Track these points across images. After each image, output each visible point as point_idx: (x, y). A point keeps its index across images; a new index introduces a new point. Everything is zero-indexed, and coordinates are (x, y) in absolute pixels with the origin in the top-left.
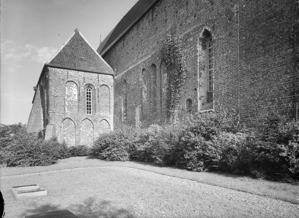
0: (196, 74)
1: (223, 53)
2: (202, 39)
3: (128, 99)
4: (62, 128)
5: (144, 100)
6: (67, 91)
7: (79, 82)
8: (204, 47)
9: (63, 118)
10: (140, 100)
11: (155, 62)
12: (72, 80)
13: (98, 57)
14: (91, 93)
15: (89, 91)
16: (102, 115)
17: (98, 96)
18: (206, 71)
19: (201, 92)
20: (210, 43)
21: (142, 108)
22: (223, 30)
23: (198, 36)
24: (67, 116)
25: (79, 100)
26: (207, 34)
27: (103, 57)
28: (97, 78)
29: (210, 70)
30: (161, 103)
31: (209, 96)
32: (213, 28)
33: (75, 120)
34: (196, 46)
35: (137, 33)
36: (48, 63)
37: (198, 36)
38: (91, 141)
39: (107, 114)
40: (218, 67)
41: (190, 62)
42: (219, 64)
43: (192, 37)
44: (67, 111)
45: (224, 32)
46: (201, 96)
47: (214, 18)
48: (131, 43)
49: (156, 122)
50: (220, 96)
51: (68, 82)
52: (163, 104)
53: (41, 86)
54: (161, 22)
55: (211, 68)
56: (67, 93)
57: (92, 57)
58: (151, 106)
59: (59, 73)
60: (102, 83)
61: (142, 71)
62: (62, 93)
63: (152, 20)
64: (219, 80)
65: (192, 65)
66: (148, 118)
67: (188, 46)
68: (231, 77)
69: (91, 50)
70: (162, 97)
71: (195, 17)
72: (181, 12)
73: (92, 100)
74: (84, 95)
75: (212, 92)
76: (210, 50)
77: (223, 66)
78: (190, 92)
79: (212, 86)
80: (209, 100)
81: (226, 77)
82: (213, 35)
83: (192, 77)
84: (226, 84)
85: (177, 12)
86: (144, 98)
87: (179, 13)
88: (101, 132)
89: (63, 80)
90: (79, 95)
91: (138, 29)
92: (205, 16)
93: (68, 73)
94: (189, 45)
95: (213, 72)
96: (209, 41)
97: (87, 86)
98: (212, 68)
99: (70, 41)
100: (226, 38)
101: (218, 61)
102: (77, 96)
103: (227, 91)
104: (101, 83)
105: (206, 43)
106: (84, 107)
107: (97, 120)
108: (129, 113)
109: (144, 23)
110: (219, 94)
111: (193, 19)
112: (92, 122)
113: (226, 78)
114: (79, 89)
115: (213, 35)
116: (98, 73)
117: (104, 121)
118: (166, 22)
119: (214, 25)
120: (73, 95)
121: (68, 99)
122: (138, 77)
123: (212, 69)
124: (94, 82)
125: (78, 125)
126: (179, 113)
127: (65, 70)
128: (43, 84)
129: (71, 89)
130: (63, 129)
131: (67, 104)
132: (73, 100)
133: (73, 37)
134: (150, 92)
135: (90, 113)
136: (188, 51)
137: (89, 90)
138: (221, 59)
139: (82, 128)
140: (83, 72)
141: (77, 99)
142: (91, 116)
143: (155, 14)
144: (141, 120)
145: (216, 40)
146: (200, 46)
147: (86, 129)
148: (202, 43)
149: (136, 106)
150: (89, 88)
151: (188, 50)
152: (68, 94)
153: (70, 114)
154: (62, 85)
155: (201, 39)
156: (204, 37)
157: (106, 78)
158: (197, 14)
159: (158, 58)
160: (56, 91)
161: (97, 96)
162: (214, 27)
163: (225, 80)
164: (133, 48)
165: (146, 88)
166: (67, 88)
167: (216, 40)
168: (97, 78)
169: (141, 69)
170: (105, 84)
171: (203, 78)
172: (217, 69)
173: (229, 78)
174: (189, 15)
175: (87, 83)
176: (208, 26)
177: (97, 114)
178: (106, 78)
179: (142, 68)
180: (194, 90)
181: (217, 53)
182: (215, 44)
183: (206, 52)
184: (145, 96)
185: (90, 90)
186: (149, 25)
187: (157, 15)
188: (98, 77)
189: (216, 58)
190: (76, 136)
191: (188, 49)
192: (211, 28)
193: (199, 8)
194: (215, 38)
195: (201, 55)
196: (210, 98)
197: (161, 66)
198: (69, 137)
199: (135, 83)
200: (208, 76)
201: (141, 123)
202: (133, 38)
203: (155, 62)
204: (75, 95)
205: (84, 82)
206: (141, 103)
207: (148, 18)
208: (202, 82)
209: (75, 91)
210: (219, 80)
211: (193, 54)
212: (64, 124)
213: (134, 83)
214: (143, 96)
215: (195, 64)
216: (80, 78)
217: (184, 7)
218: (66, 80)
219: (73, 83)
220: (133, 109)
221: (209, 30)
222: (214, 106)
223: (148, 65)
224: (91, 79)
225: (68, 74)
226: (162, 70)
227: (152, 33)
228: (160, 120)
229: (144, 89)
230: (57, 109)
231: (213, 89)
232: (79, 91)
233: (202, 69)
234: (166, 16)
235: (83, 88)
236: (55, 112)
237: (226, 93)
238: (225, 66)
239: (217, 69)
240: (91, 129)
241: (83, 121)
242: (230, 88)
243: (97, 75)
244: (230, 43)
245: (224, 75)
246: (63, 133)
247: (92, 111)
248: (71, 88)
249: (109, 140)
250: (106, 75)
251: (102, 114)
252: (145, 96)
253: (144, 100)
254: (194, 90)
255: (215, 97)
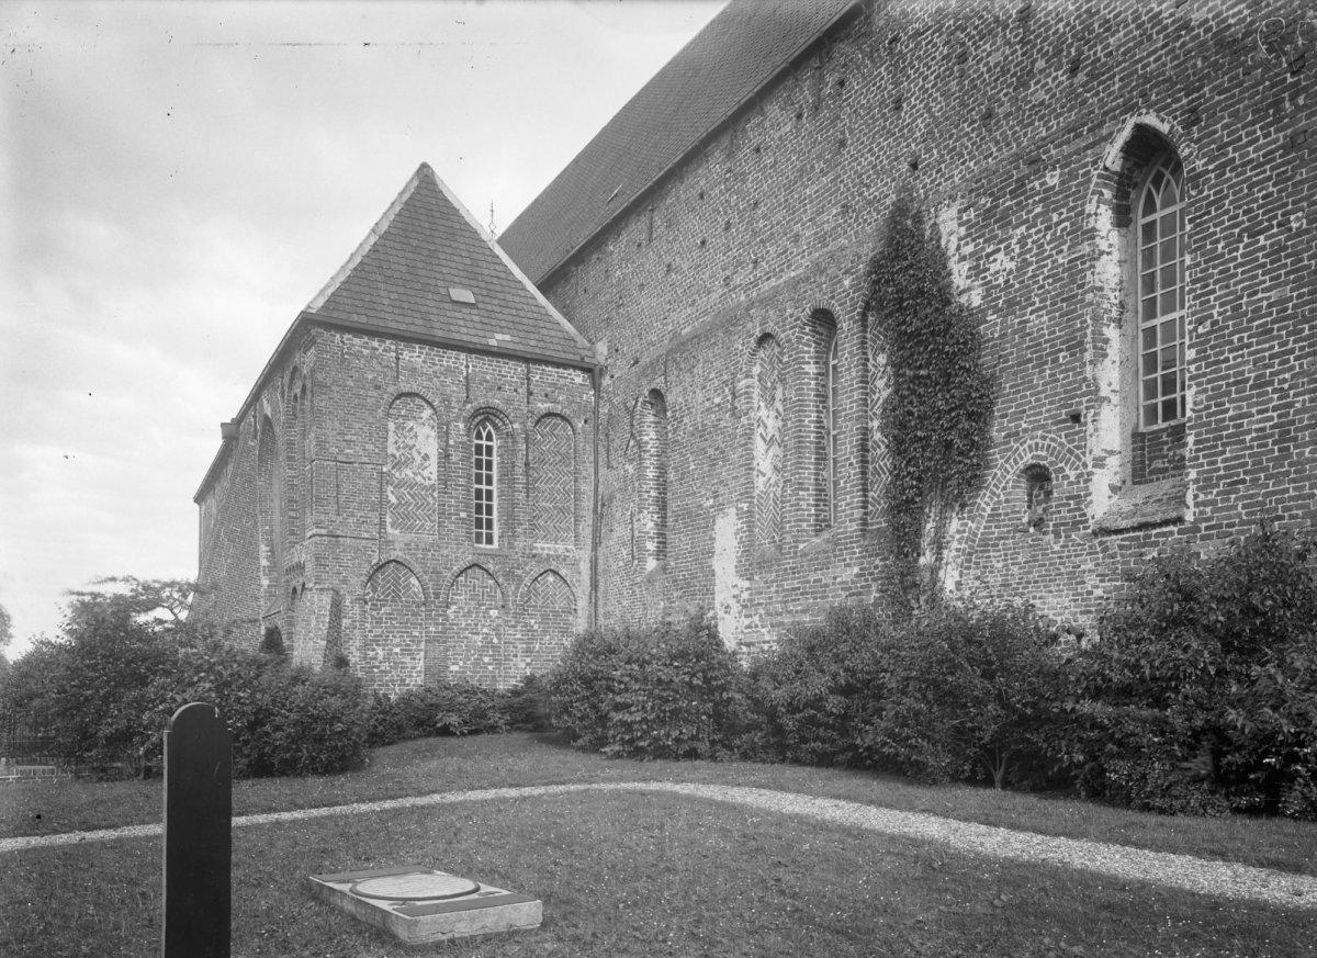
0: (1081, 343)
1: (1254, 235)
2: (1115, 173)
3: (672, 476)
4: (368, 607)
5: (760, 483)
6: (392, 438)
7: (446, 400)
8: (1122, 218)
9: (374, 561)
10: (742, 480)
11: (833, 298)
12: (415, 388)
13: (524, 289)
14: (495, 450)
15: (484, 443)
16: (543, 549)
17: (527, 464)
18: (1128, 328)
19: (1110, 431)
20: (1150, 194)
21: (748, 517)
22: (1253, 123)
23: (1095, 163)
24: (392, 552)
25: (444, 479)
26: (1148, 152)
27: (546, 286)
28: (522, 384)
29: (1149, 324)
30: (865, 490)
31: (1143, 449)
32: (1192, 118)
33: (426, 572)
34: (1082, 212)
35: (729, 171)
36: (313, 311)
37: (1095, 163)
38: (490, 668)
39: (561, 548)
40: (1221, 305)
41: (1042, 287)
42: (1227, 287)
43: (1054, 169)
44: (389, 530)
45: (1262, 128)
46: (1106, 451)
47: (1195, 65)
48: (693, 224)
49: (835, 578)
50: (1228, 444)
51: (397, 398)
52: (871, 494)
53: (266, 417)
54: (870, 109)
55: (1174, 310)
56: (391, 449)
57: (498, 288)
58: (805, 507)
59: (358, 355)
60: (544, 407)
61: (753, 343)
62: (372, 447)
63: (817, 108)
64: (1228, 368)
65: (1053, 304)
66: (789, 563)
67: (1028, 212)
68: (1302, 348)
69: (490, 259)
70: (867, 462)
71: (1074, 71)
72: (989, 54)
73: (500, 481)
74: (465, 459)
75: (1184, 424)
76: (1149, 230)
77: (1249, 296)
78: (1040, 433)
79: (1183, 398)
80: (1143, 469)
81: (1272, 347)
82: (1187, 151)
83: (1055, 360)
84: (1271, 383)
85: (962, 58)
86: (761, 468)
87: (978, 63)
88: (536, 627)
89: (378, 387)
90: (447, 456)
91: (730, 155)
92: (1140, 60)
93: (398, 359)
94: (1039, 210)
95: (1188, 328)
96: (1149, 184)
97: (479, 418)
98: (1182, 307)
99: (399, 215)
100: (1274, 159)
101: (1221, 273)
102: (434, 460)
103: (1279, 416)
104: (539, 405)
105: (1132, 196)
106: (463, 515)
107: (519, 572)
108: (680, 541)
109: (767, 124)
110: (1228, 436)
111: (1061, 83)
112: (500, 580)
113: (1272, 357)
114: (444, 435)
115: (1184, 151)
116: (527, 360)
117: (551, 578)
118: (898, 108)
119: (1193, 101)
120: (418, 459)
121: (397, 475)
122: (734, 375)
123: (1184, 312)
124: (508, 401)
125: (437, 595)
126: (976, 535)
127: (388, 342)
128: (273, 409)
129: (412, 429)
130: (374, 613)
131: (393, 500)
132: (419, 479)
133: (411, 198)
134: (800, 440)
135: (490, 540)
136: (1030, 236)
137: (484, 435)
138: (1242, 265)
139: (454, 608)
140: (463, 356)
141: (434, 477)
142: (493, 556)
143: (831, 79)
144: (746, 571)
145: (1207, 172)
146: (1103, 208)
147: (469, 611)
148: (1116, 197)
149: (720, 507)
150: (484, 429)
151: (1033, 230)
152: (395, 452)
153: (402, 545)
154: (372, 411)
155: (1107, 176)
156: (1128, 165)
157: (562, 381)
158: (1088, 57)
159: (847, 283)
160: (347, 438)
161: (520, 463)
162: (1193, 111)
163: (1266, 366)
164: (703, 243)
165: (772, 424)
166: (391, 426)
167: (1207, 172)
168: (522, 384)
169: (751, 336)
170: (558, 409)
171: (1114, 362)
172: (1215, 312)
173: (1292, 351)
174: (1040, 64)
175: (482, 402)
176: (1158, 111)
177: (521, 545)
178: (562, 381)
179: (758, 333)
180: (1065, 421)
181: (1215, 233)
182: (1201, 192)
183: (1130, 236)
184: (765, 459)
185: (489, 438)
186: (798, 130)
187: (842, 83)
188: (528, 379)
189: (1206, 262)
190: (431, 647)
191: (1028, 229)
192: (1175, 118)
193: (1100, 26)
194: (1199, 163)
195: (1109, 253)
196: (1151, 460)
197: (864, 316)
198: (397, 650)
199: (717, 400)
200: (1141, 352)
201: (747, 584)
202: (701, 196)
203: (833, 298)
204: (426, 457)
205: (468, 400)
206: (747, 494)
207: (790, 102)
208: (1110, 384)
209: (427, 441)
210: (1228, 368)
211: (1065, 247)
212: (375, 590)
213: (707, 404)
214: (755, 462)
215: (1076, 296)
216: (449, 381)
217: (1004, 29)
218: (391, 389)
219: (417, 401)
220: (702, 523)
221: (1164, 128)
222: (1196, 496)
223: (791, 316)
224: (499, 388)
225: (401, 363)
226: (868, 336)
227: (812, 167)
228: (856, 570)
229: (761, 430)
230: (350, 520)
231: (1189, 413)
232: (447, 442)
233: (1110, 319)
234: (897, 84)
235: (461, 425)
236: (339, 533)
237: (1272, 427)
238: (1268, 298)
239: (1215, 312)
240: (491, 612)
241: (460, 579)
242: (1298, 405)
243: (521, 368)
244: (1302, 182)
245: (1258, 343)
246: (371, 631)
247: (496, 532)
248: (411, 424)
249: (431, 699)
250: (561, 370)
251: (543, 547)
252: (765, 459)
253: (762, 479)
254: (1065, 421)
255: (1197, 450)
